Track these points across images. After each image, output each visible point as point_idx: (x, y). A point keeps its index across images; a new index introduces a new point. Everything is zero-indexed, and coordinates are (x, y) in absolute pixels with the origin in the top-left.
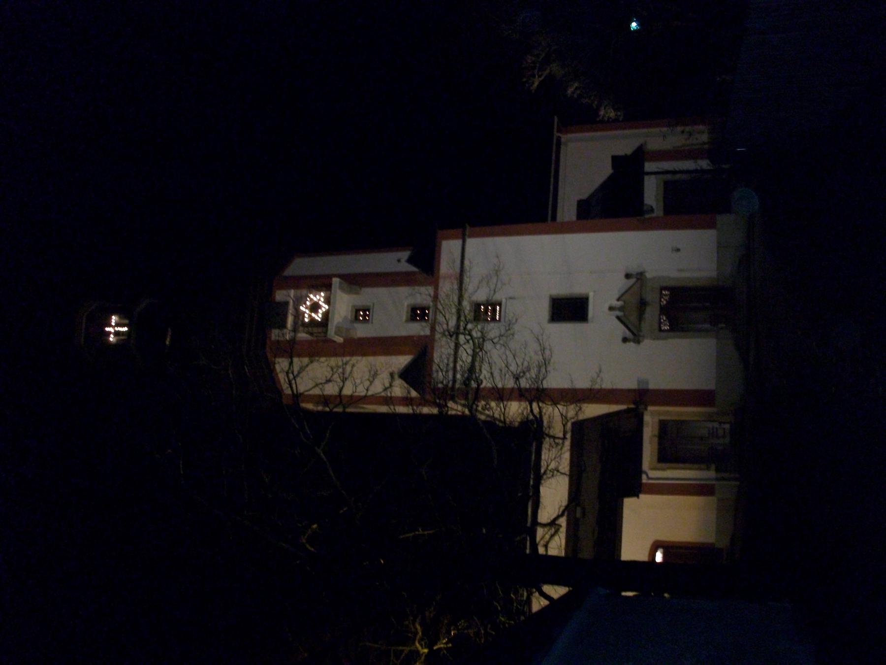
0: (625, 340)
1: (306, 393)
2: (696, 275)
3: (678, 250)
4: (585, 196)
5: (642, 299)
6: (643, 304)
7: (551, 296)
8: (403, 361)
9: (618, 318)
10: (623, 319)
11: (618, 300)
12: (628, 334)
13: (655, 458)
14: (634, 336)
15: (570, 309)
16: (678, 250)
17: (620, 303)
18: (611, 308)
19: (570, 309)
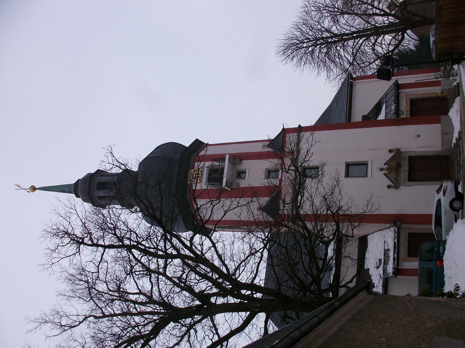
0: (389, 187)
1: (388, 225)
2: (430, 149)
3: (419, 136)
4: (366, 114)
5: (398, 164)
6: (399, 166)
7: (346, 162)
8: (264, 200)
9: (384, 174)
10: (388, 175)
11: (385, 164)
12: (390, 183)
13: (412, 97)
14: (395, 185)
15: (355, 169)
16: (419, 136)
17: (386, 166)
18: (381, 169)
19: (355, 169)
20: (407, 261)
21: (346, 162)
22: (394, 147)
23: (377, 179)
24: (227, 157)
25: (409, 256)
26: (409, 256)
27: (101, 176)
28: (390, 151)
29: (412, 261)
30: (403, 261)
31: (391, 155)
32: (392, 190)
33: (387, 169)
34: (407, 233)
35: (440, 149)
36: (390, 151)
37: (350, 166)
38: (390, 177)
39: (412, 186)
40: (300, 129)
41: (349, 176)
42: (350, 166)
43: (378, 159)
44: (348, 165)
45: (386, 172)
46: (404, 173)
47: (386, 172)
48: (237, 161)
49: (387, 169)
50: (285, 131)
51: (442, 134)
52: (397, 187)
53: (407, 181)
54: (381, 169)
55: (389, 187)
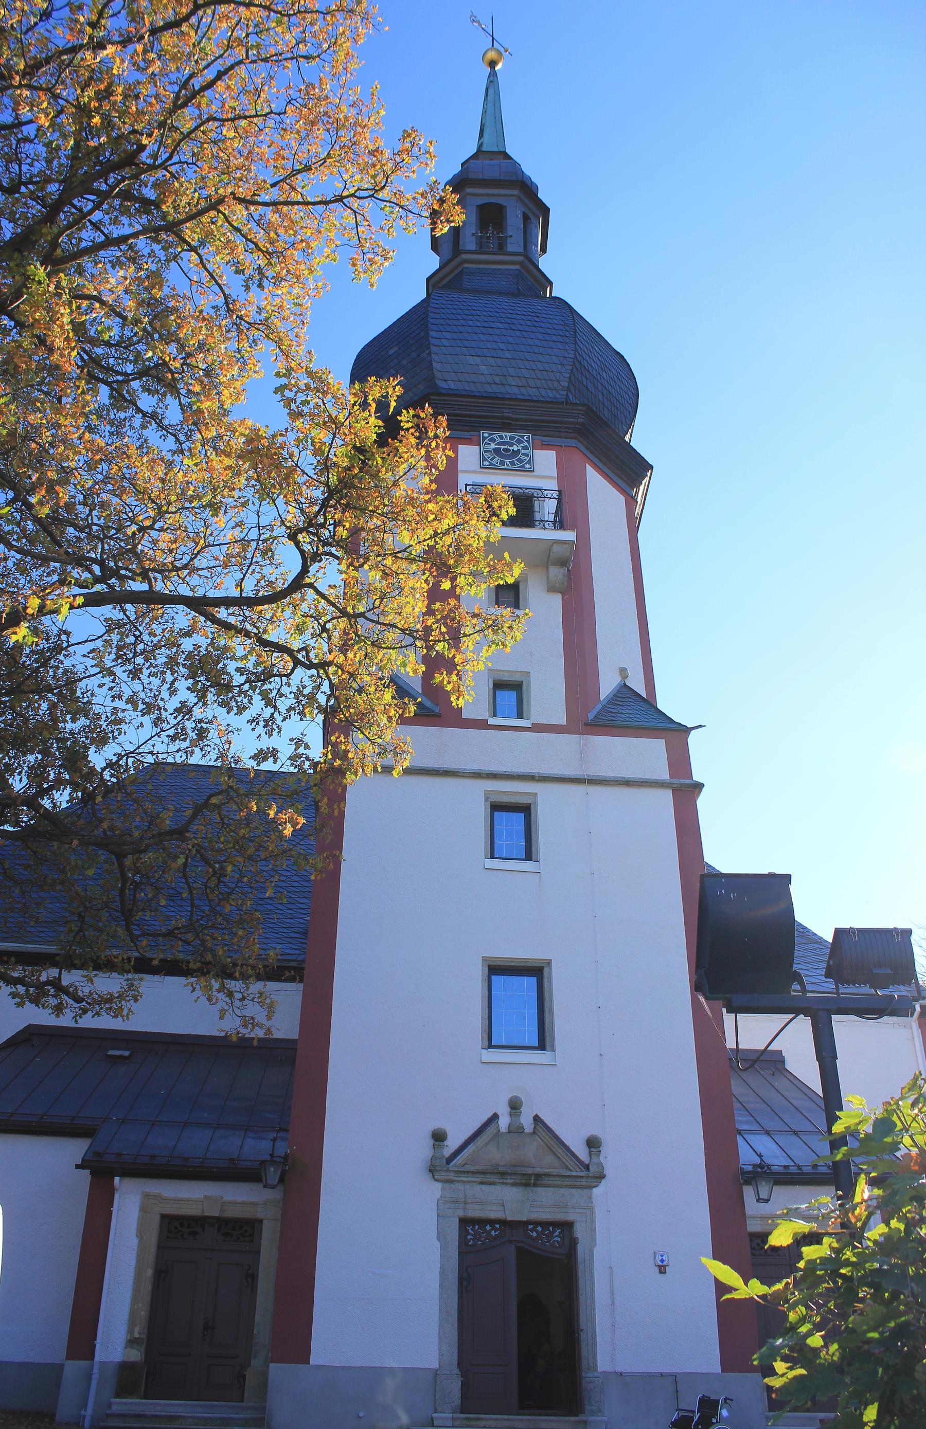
0: (439, 1137)
3: (662, 1269)
7: (549, 963)
9: (495, 1117)
11: (537, 1119)
12: (453, 1142)
13: (532, 807)
14: (446, 1162)
16: (662, 1269)
17: (526, 1121)
18: (515, 1106)
20: (144, 1210)
21: (549, 963)
22: (609, 1158)
23: (473, 1090)
24: (569, 536)
25: (465, 1222)
26: (465, 1222)
27: (526, 218)
28: (593, 1144)
29: (140, 1234)
30: (146, 1196)
31: (581, 1152)
32: (424, 1150)
33: (516, 1130)
34: (259, 1215)
35: (603, 1363)
36: (593, 1144)
37: (533, 980)
38: (481, 1140)
39: (441, 1235)
40: (686, 792)
41: (494, 978)
42: (533, 980)
43: (562, 1094)
44: (536, 971)
45: (504, 1122)
46: (505, 1202)
47: (504, 1122)
48: (557, 573)
49: (516, 1130)
50: (676, 734)
51: (675, 1377)
52: (437, 1168)
53: (461, 1213)
54: (515, 1106)
55: (439, 1137)
